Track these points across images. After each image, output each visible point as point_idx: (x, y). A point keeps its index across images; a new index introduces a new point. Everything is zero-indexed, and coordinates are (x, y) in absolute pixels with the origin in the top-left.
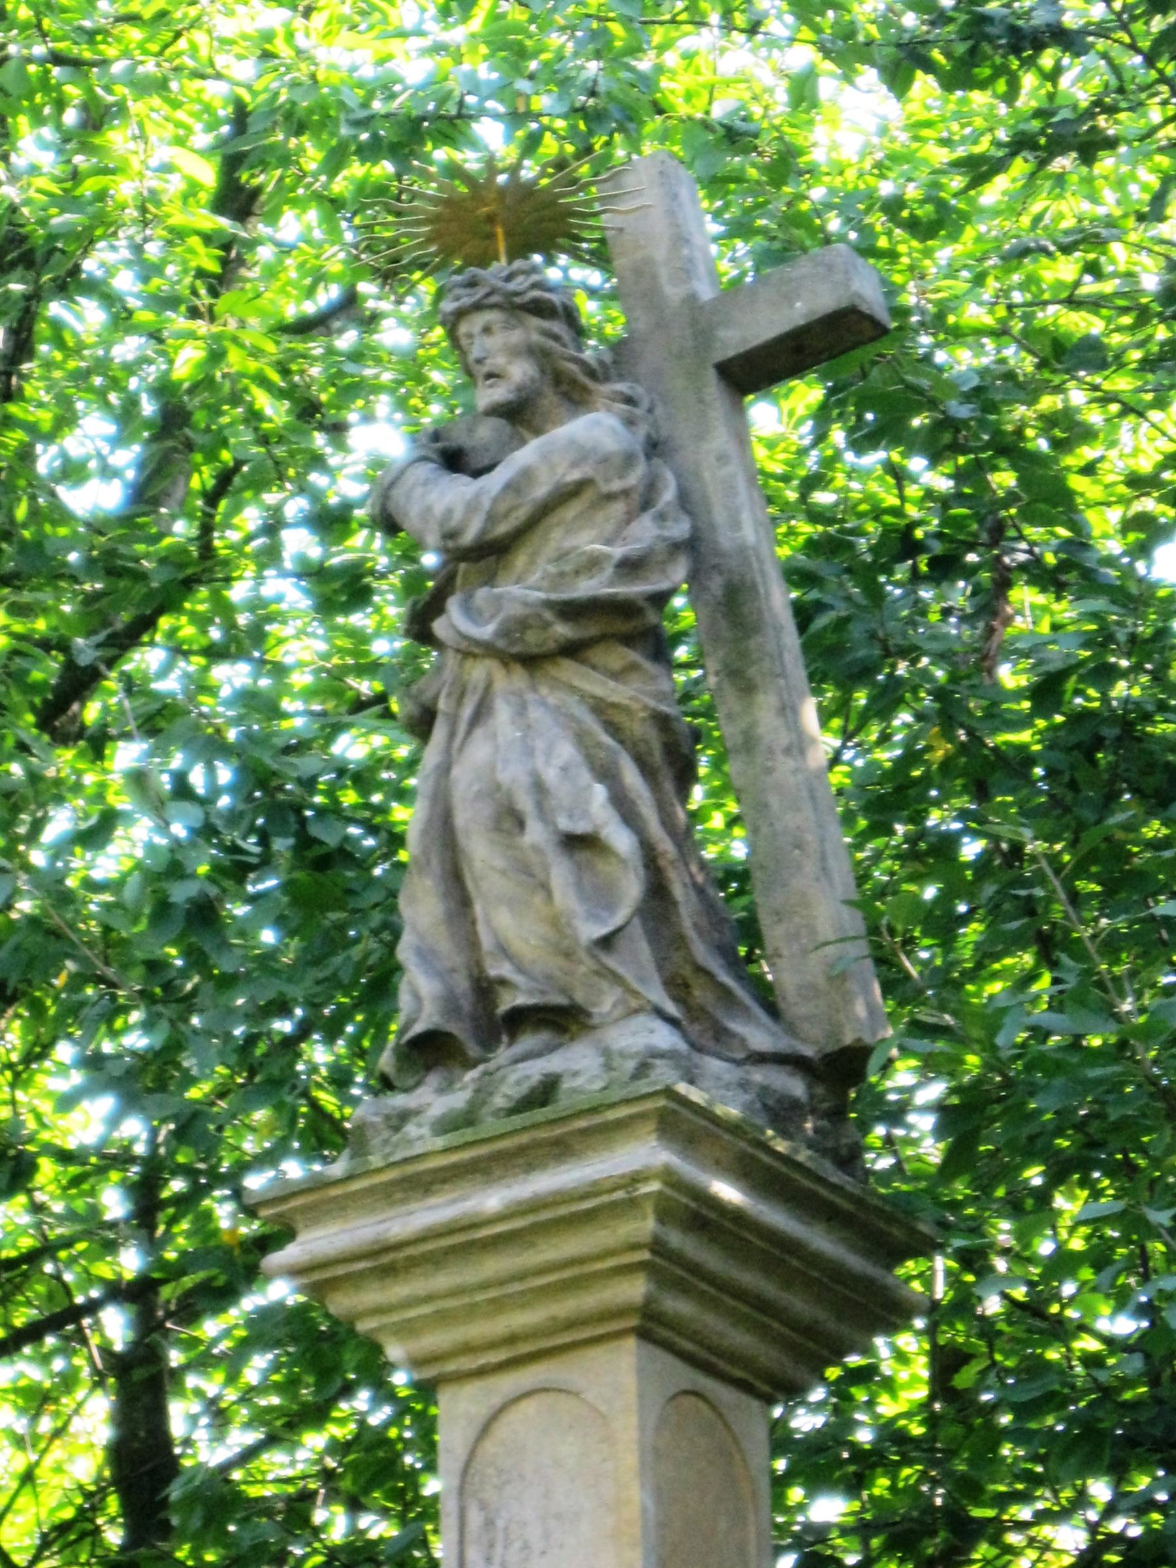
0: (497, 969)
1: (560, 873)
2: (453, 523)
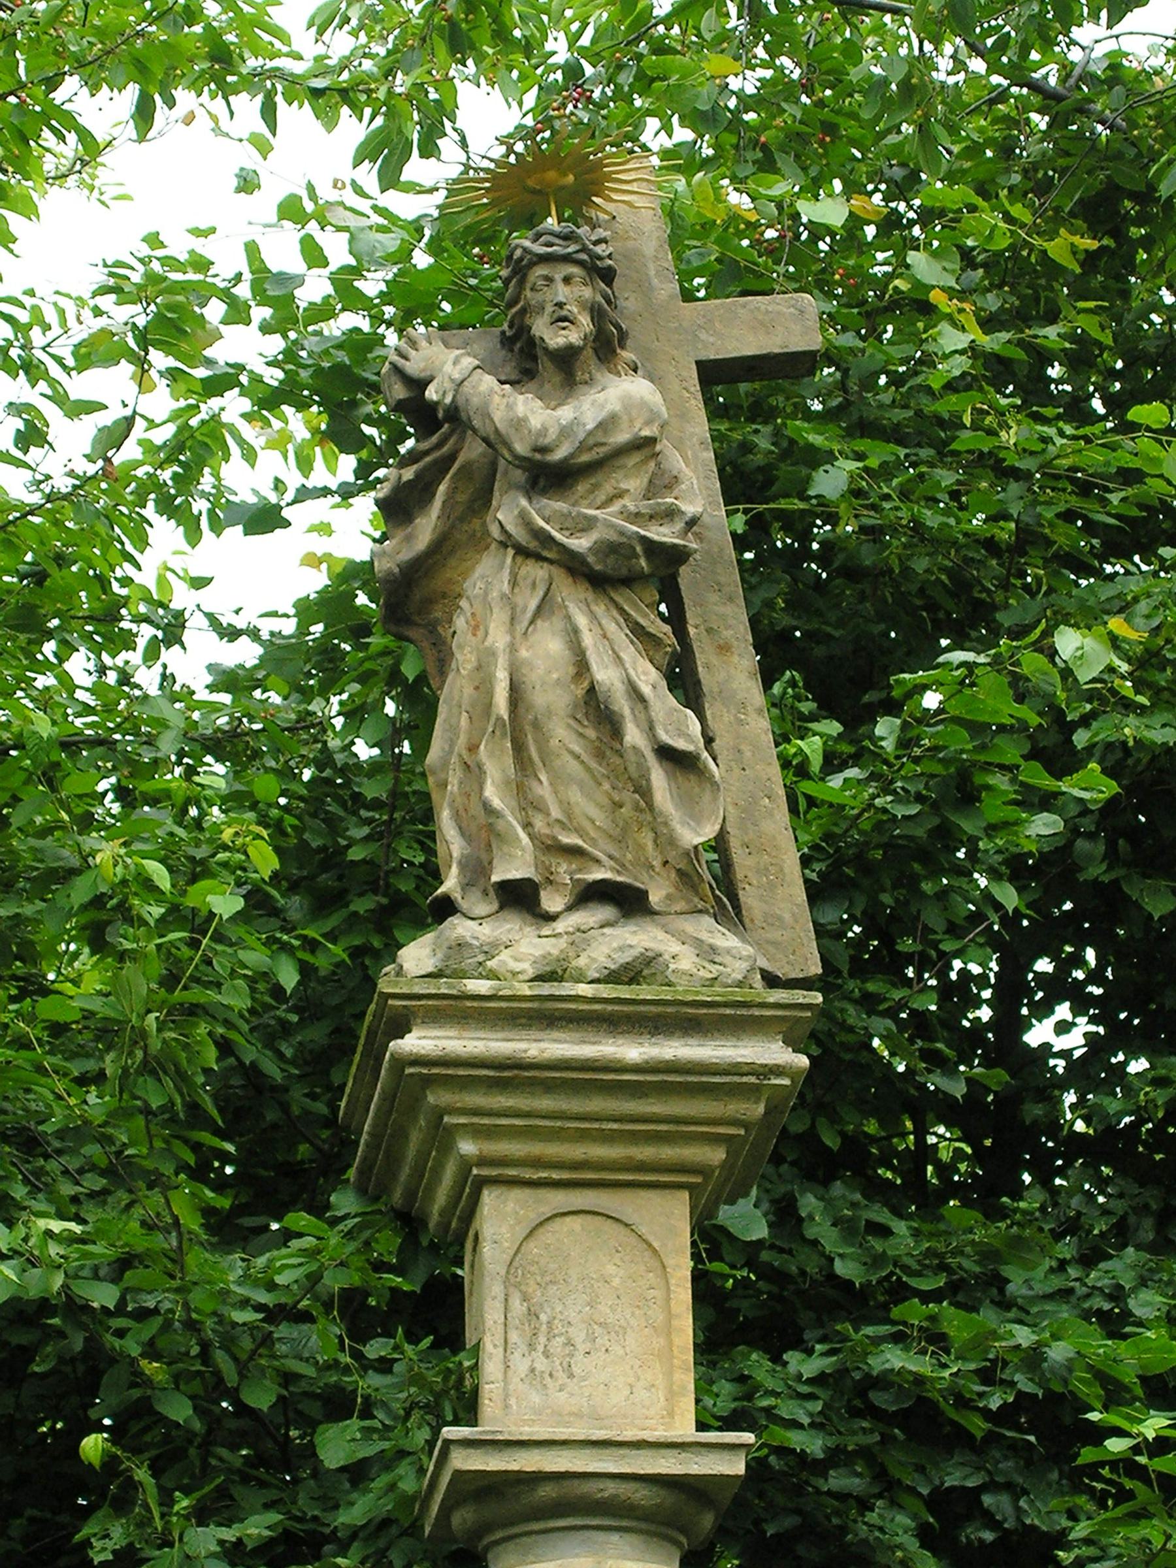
2: (547, 441)
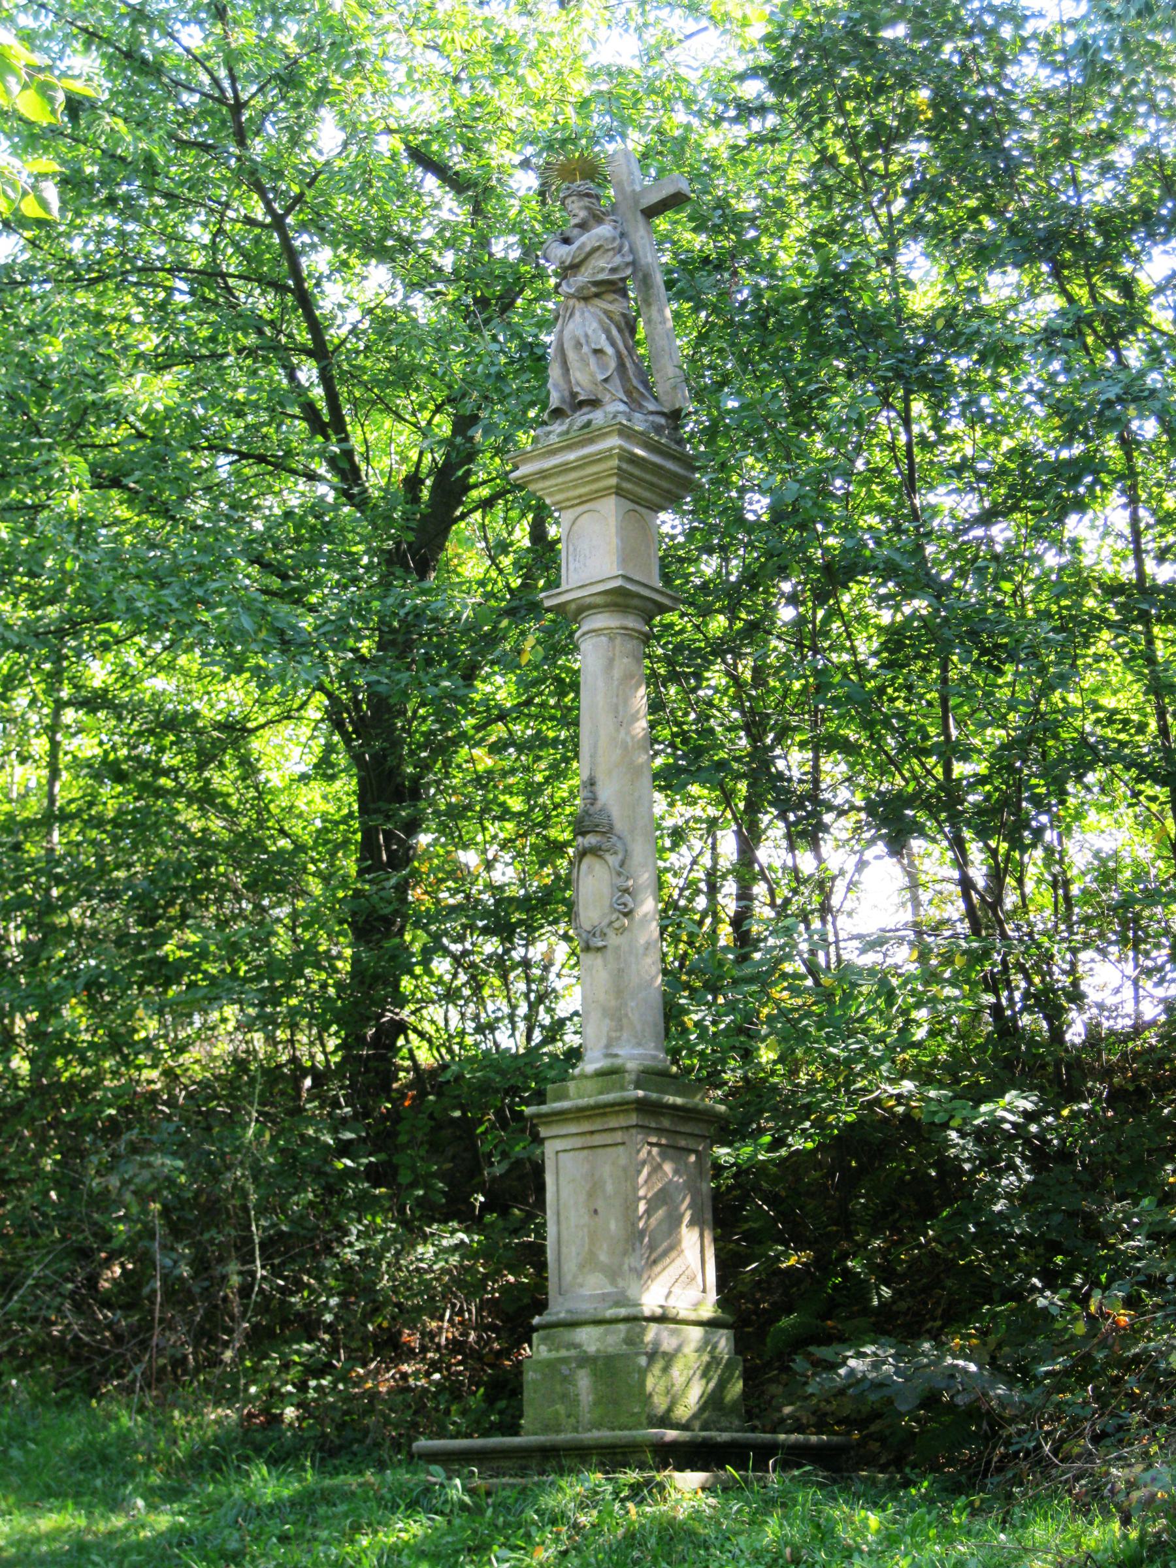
0: (577, 389)
1: (592, 360)
